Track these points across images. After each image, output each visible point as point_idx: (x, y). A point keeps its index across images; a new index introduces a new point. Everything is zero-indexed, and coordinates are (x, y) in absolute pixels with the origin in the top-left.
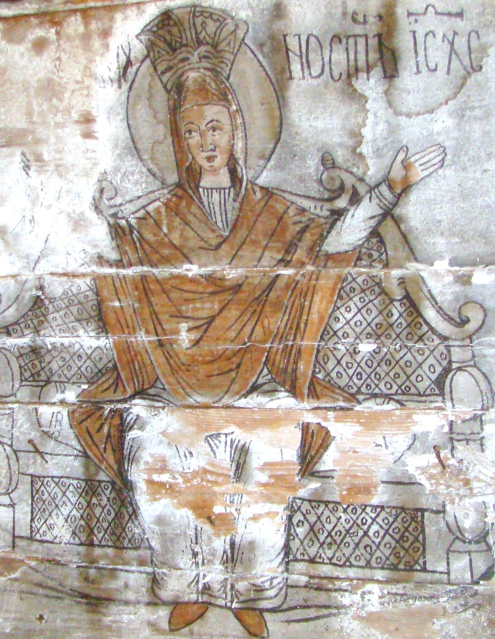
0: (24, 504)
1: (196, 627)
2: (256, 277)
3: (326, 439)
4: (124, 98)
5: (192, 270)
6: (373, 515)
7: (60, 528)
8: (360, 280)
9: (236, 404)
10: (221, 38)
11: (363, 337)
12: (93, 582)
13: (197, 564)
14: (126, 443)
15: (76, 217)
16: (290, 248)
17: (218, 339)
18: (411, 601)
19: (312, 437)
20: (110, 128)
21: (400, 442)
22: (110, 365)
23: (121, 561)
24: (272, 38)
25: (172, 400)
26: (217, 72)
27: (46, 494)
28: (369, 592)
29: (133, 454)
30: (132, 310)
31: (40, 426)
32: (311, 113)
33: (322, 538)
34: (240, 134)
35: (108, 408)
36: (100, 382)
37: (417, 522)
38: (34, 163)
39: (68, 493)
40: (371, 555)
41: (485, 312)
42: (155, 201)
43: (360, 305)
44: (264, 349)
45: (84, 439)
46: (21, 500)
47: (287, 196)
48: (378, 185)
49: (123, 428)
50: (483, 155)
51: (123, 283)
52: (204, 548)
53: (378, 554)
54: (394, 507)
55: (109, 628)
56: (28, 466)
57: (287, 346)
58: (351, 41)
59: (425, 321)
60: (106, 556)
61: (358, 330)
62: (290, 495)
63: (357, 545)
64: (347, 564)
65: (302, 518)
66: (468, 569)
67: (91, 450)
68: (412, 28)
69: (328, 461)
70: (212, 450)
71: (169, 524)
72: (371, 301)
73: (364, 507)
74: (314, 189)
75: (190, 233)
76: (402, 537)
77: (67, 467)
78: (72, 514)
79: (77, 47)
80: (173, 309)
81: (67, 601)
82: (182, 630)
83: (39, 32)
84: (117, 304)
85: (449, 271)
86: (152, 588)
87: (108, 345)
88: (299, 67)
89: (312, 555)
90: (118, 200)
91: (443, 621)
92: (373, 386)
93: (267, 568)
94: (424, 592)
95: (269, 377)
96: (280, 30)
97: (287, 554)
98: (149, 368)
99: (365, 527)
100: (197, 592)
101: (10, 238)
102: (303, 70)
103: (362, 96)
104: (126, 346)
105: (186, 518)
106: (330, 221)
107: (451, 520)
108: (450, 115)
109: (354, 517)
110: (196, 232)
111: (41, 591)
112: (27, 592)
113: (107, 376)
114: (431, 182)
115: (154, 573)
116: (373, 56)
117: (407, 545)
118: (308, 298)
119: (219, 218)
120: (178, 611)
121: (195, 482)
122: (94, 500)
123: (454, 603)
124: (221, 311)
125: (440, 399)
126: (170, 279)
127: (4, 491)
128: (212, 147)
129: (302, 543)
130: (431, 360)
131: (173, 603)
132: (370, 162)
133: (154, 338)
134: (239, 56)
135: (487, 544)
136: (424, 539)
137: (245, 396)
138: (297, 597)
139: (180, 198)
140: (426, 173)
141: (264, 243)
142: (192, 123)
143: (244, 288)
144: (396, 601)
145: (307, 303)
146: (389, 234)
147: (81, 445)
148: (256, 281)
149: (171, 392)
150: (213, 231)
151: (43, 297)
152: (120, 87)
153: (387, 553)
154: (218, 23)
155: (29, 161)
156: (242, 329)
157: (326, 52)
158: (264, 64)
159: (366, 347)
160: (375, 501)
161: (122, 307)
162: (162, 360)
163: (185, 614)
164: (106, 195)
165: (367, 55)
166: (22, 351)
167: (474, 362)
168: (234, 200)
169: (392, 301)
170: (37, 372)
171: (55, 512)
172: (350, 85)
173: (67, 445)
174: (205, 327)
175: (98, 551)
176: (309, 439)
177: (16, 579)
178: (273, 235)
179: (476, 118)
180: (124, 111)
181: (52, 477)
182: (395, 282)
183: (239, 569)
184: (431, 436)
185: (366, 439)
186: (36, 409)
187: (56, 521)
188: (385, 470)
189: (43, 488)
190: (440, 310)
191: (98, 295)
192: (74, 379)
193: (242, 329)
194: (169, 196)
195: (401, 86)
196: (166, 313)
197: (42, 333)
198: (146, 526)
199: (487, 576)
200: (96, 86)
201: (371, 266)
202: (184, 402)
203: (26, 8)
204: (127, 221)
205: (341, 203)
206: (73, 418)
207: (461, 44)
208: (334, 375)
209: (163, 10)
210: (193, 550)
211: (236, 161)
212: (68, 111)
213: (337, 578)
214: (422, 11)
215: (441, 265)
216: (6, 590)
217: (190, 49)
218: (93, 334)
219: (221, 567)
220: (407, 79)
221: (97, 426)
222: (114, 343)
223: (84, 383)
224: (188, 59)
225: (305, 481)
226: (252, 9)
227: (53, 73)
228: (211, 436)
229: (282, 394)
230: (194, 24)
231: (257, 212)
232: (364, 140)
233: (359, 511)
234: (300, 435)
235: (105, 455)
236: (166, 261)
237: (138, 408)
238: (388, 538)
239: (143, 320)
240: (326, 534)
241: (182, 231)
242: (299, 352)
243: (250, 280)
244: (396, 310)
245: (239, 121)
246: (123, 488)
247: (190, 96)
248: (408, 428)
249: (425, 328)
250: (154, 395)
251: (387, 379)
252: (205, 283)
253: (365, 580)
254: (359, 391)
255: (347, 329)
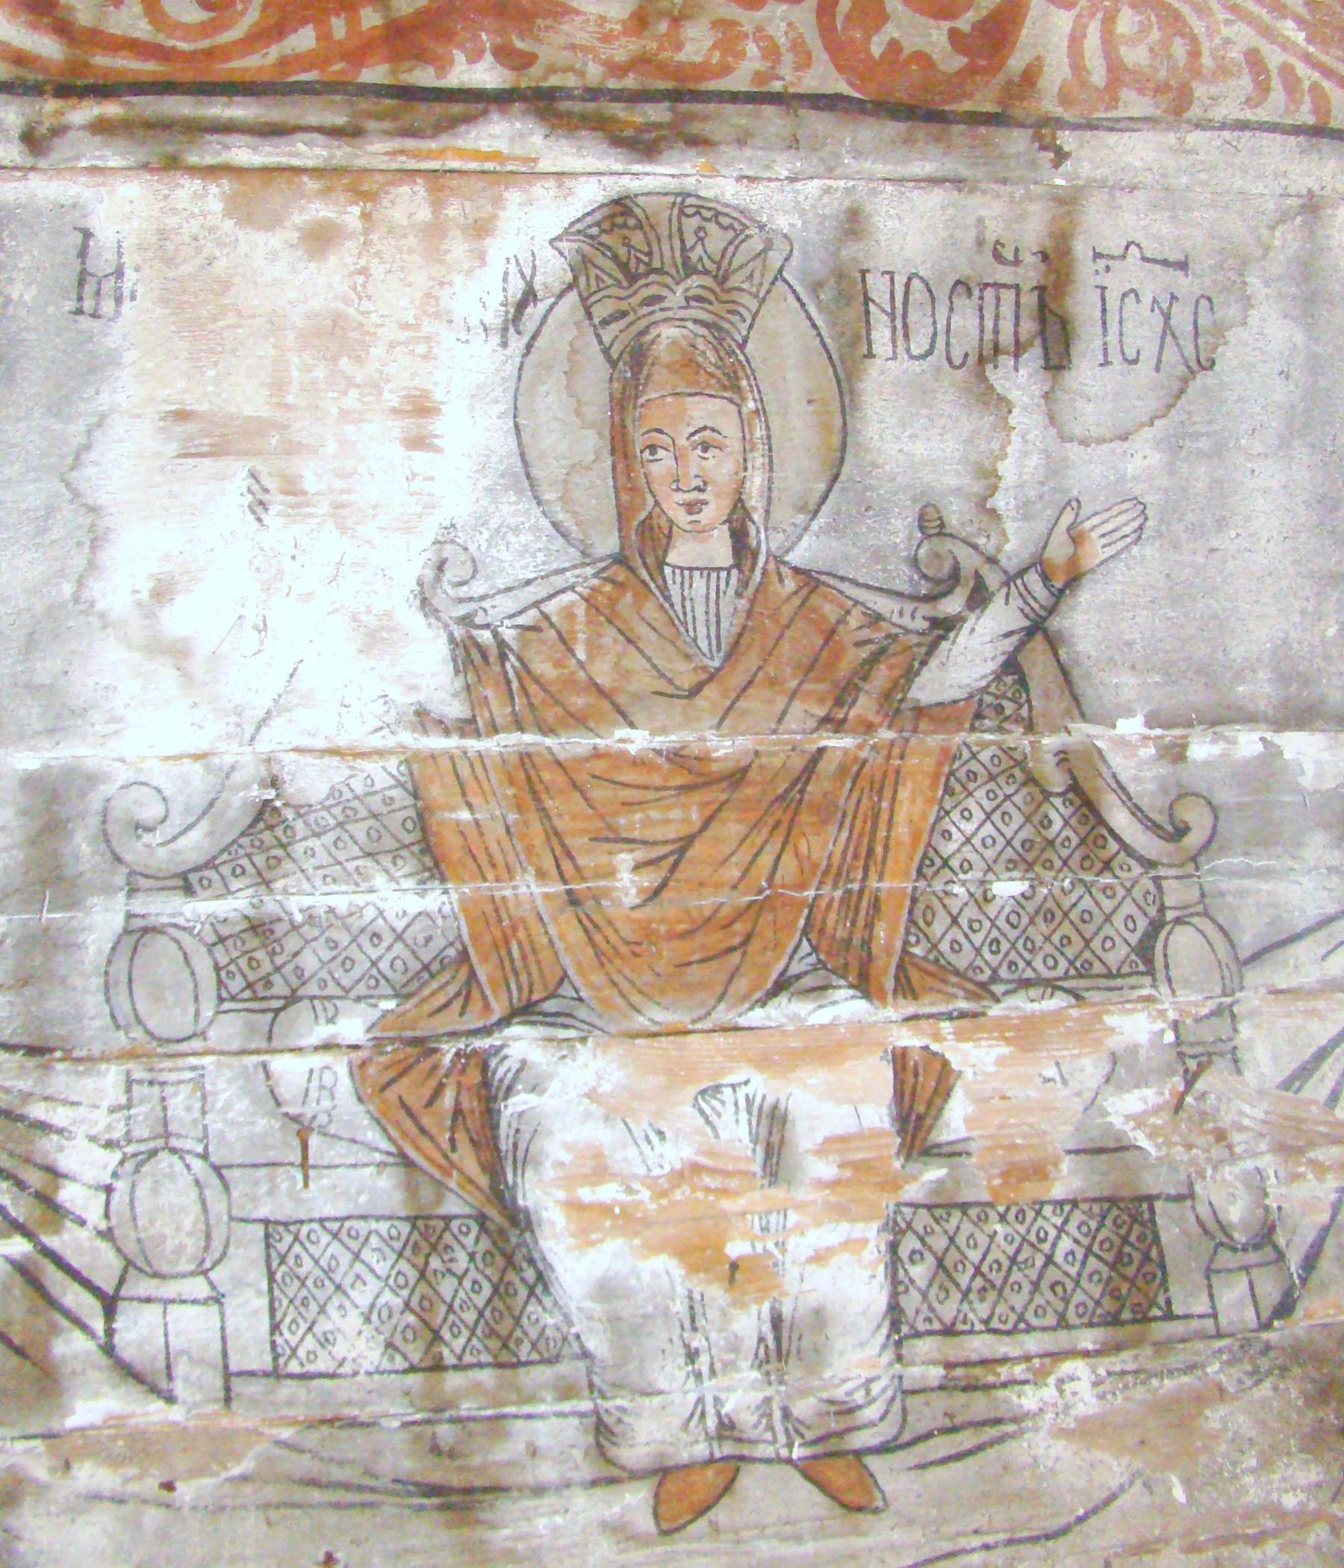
0: (249, 1292)
1: (720, 1514)
2: (774, 754)
3: (944, 1077)
4: (511, 368)
5: (637, 740)
6: (1058, 1221)
7: (353, 1338)
8: (985, 756)
9: (743, 1021)
10: (735, 264)
11: (999, 867)
12: (452, 1454)
13: (698, 1375)
14: (503, 1124)
15: (373, 623)
16: (845, 693)
17: (702, 884)
18: (1155, 1382)
19: (916, 1075)
20: (473, 432)
21: (1090, 1070)
22: (451, 952)
23: (514, 1397)
24: (840, 274)
25: (597, 1022)
26: (720, 329)
27: (308, 1264)
28: (1072, 1379)
29: (522, 1147)
30: (502, 830)
31: (279, 1104)
32: (903, 425)
33: (964, 1280)
34: (758, 459)
35: (448, 1050)
36: (426, 992)
37: (1143, 1224)
38: (281, 497)
39: (367, 1254)
40: (1066, 1300)
41: (1214, 809)
42: (563, 591)
43: (988, 806)
44: (802, 903)
45: (398, 1125)
46: (239, 1282)
47: (845, 587)
48: (1022, 572)
49: (489, 1094)
50: (1208, 522)
51: (479, 770)
52: (709, 1340)
53: (1079, 1297)
54: (1094, 1200)
55: (510, 1555)
56: (255, 1199)
57: (849, 892)
58: (989, 293)
59: (1111, 831)
60: (477, 1388)
61: (990, 854)
62: (886, 1202)
63: (1036, 1285)
64: (1021, 1326)
65: (918, 1245)
66: (1249, 1301)
67: (418, 1148)
68: (1099, 280)
69: (956, 1119)
70: (708, 1121)
71: (629, 1294)
72: (1007, 797)
73: (1039, 1206)
74: (902, 578)
75: (634, 661)
76: (1120, 1255)
77: (359, 1193)
78: (382, 1301)
79: (411, 251)
80: (597, 824)
81: (388, 1510)
82: (691, 1528)
83: (320, 210)
84: (465, 815)
85: (1146, 738)
86: (599, 1446)
87: (447, 909)
88: (888, 333)
89: (948, 1319)
90: (478, 588)
91: (1223, 1410)
92: (1021, 964)
93: (856, 1362)
94: (1177, 1358)
95: (813, 959)
96: (855, 260)
97: (895, 1326)
98: (545, 955)
99: (1046, 1247)
100: (709, 1438)
101: (197, 665)
102: (894, 341)
103: (1001, 399)
104: (489, 909)
105: (665, 1279)
106: (928, 639)
107: (1203, 1210)
108: (1157, 445)
109: (1022, 1229)
110: (649, 659)
111: (316, 1495)
112: (278, 1506)
113: (444, 978)
114: (1118, 568)
115: (596, 1412)
116: (1028, 327)
117: (1130, 1271)
118: (887, 793)
119: (702, 631)
120: (671, 1486)
121: (678, 1195)
122: (435, 1263)
123: (1235, 1372)
124: (705, 826)
125: (1147, 980)
126: (587, 760)
127: (192, 1267)
128: (698, 482)
129: (925, 1295)
130: (1128, 908)
131: (654, 1472)
132: (1010, 527)
133: (557, 888)
134: (769, 304)
135: (1275, 1247)
136: (1161, 1253)
137: (763, 1002)
138: (927, 1414)
139: (620, 586)
140: (1110, 551)
141: (794, 684)
142: (660, 431)
143: (752, 775)
144: (1126, 1386)
145: (885, 804)
146: (1038, 667)
147: (390, 1138)
148: (777, 763)
149: (594, 1004)
150: (688, 657)
151: (278, 804)
152: (504, 345)
153: (1096, 1291)
154: (731, 234)
155: (266, 491)
156: (752, 863)
157: (942, 312)
158: (819, 323)
159: (1008, 888)
160: (1058, 1191)
161: (477, 822)
162: (576, 935)
163: (689, 1492)
164: (450, 574)
165: (1017, 325)
166: (224, 931)
167: (1203, 908)
168: (739, 595)
169: (1047, 795)
170: (262, 976)
171: (336, 1301)
172: (982, 377)
173: (354, 1141)
174: (671, 859)
175: (454, 1381)
176: (910, 1079)
177: (244, 1478)
178: (811, 668)
179: (1200, 453)
180: (510, 396)
181: (322, 1221)
182: (1051, 761)
183: (795, 1372)
184: (1142, 1052)
185: (1022, 1070)
186: (265, 1066)
187: (340, 1323)
188: (1070, 1128)
189: (297, 1249)
190: (1136, 811)
191: (415, 795)
192: (361, 989)
193: (752, 863)
194: (596, 582)
195: (1074, 386)
196: (582, 832)
197: (279, 885)
198: (573, 1306)
199: (1285, 1308)
200: (447, 337)
201: (1000, 729)
202: (625, 1025)
203: (297, 155)
204: (496, 634)
205: (952, 605)
206: (364, 1078)
207: (1182, 319)
208: (944, 946)
209: (614, 194)
210: (687, 1346)
211: (747, 514)
212: (376, 387)
213: (1004, 1360)
214: (1118, 252)
215: (1131, 726)
216: (222, 1509)
217: (668, 280)
218: (409, 883)
219: (755, 1374)
220: (1084, 372)
221: (427, 1092)
222: (461, 901)
223: (386, 997)
224: (660, 299)
225: (913, 1167)
226: (803, 213)
227: (348, 302)
228: (703, 1092)
229: (843, 993)
230: (680, 231)
231: (784, 621)
232: (1002, 484)
233: (1030, 1215)
234: (890, 1074)
235: (454, 1157)
236: (580, 720)
237: (522, 1043)
238: (1092, 1262)
239: (529, 850)
240: (971, 1271)
241: (620, 656)
242: (876, 905)
243: (764, 760)
244: (1058, 813)
245: (759, 433)
246: (507, 1228)
247: (660, 375)
248: (1099, 1042)
249: (1113, 846)
250: (557, 1014)
251: (1048, 948)
252: (666, 766)
253: (1058, 1356)
254: (995, 978)
255: (968, 852)
